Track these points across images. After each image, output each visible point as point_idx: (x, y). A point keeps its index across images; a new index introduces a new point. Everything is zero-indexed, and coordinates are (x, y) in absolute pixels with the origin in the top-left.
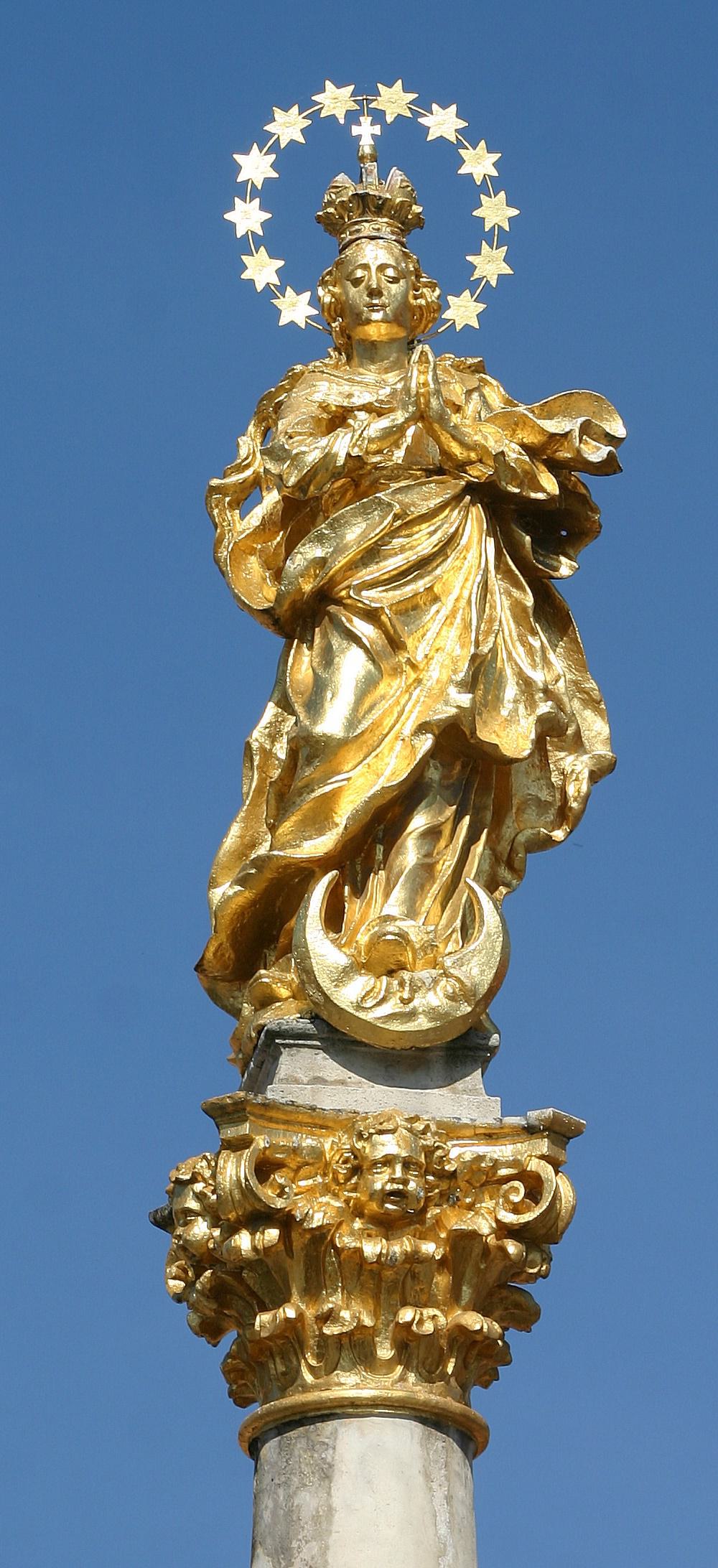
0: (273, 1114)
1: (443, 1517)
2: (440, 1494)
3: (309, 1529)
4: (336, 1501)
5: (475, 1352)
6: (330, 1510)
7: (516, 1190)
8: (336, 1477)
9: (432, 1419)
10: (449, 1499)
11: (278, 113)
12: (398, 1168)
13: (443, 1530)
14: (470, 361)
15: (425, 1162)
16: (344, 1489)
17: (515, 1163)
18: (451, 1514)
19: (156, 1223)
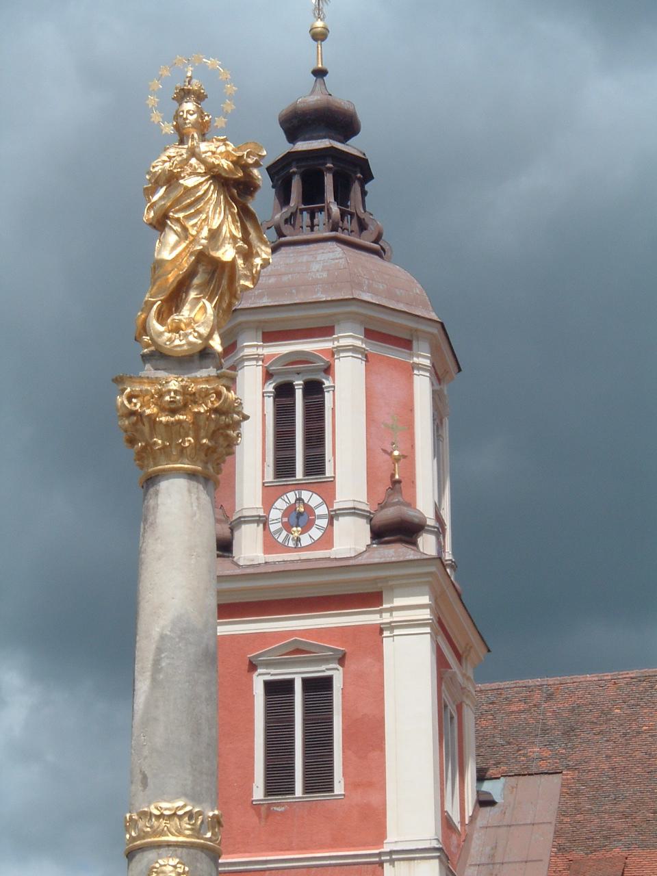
0: (390, 583)
1: (195, 504)
2: (194, 497)
3: (152, 511)
4: (159, 502)
5: (210, 451)
6: (157, 505)
7: (213, 397)
8: (160, 495)
9: (192, 475)
10: (198, 499)
11: (153, 119)
12: (172, 394)
13: (195, 508)
14: (222, 138)
15: (184, 391)
16: (162, 498)
17: (213, 389)
18: (199, 504)
19: (113, 380)
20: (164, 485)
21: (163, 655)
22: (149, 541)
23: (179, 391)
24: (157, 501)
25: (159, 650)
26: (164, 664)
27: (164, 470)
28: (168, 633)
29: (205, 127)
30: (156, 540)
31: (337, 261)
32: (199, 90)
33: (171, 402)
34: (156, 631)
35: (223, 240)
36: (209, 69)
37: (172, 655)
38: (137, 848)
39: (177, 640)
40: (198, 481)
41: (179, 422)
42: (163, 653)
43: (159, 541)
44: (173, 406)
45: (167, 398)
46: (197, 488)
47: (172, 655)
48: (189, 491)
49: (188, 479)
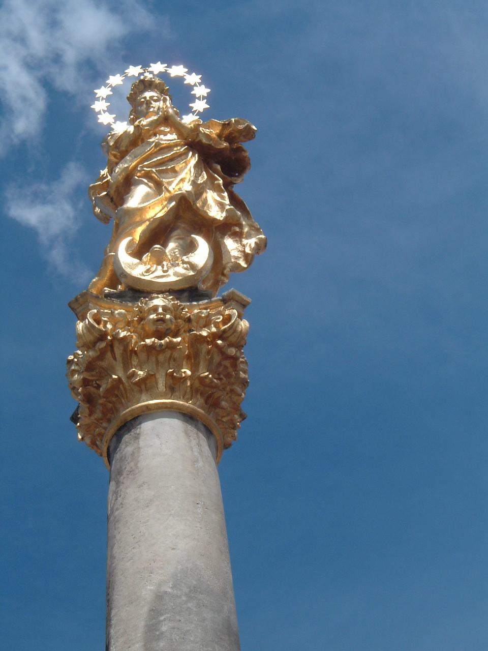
9: (189, 417)
20: (147, 426)
21: (162, 618)
22: (128, 491)
23: (169, 309)
24: (139, 444)
25: (155, 613)
26: (164, 629)
27: (148, 407)
28: (169, 590)
29: (119, 474)
30: (140, 486)
31: (169, 142)
32: (164, 114)
33: (158, 320)
34: (148, 591)
35: (193, 202)
36: (185, 83)
37: (178, 617)
38: (164, 406)
39: (184, 598)
40: (196, 427)
41: (171, 346)
42: (162, 615)
43: (145, 486)
44: (161, 327)
45: (153, 316)
46: (198, 438)
47: (178, 617)
48: (186, 433)
49: (184, 421)
